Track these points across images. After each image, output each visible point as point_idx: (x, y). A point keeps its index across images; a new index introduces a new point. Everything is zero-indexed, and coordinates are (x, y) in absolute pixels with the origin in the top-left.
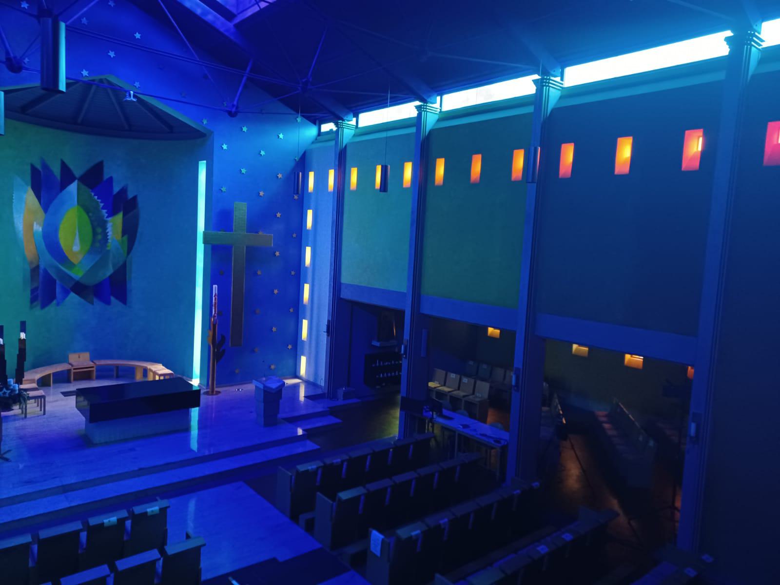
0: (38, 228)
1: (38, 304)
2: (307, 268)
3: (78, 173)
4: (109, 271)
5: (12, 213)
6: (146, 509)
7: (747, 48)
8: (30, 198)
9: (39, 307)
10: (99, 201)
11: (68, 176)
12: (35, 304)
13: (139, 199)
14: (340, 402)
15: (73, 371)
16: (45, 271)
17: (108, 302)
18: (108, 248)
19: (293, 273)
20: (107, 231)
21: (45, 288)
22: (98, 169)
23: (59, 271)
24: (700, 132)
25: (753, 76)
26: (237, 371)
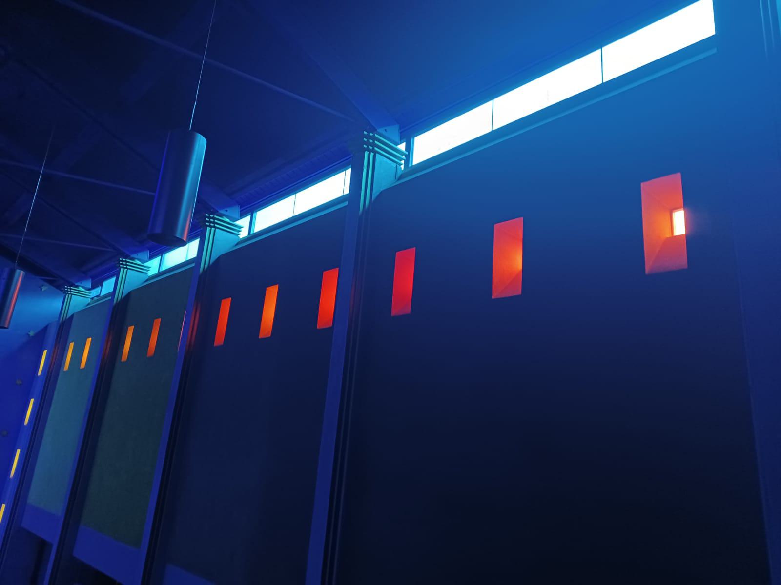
2: (10, 479)
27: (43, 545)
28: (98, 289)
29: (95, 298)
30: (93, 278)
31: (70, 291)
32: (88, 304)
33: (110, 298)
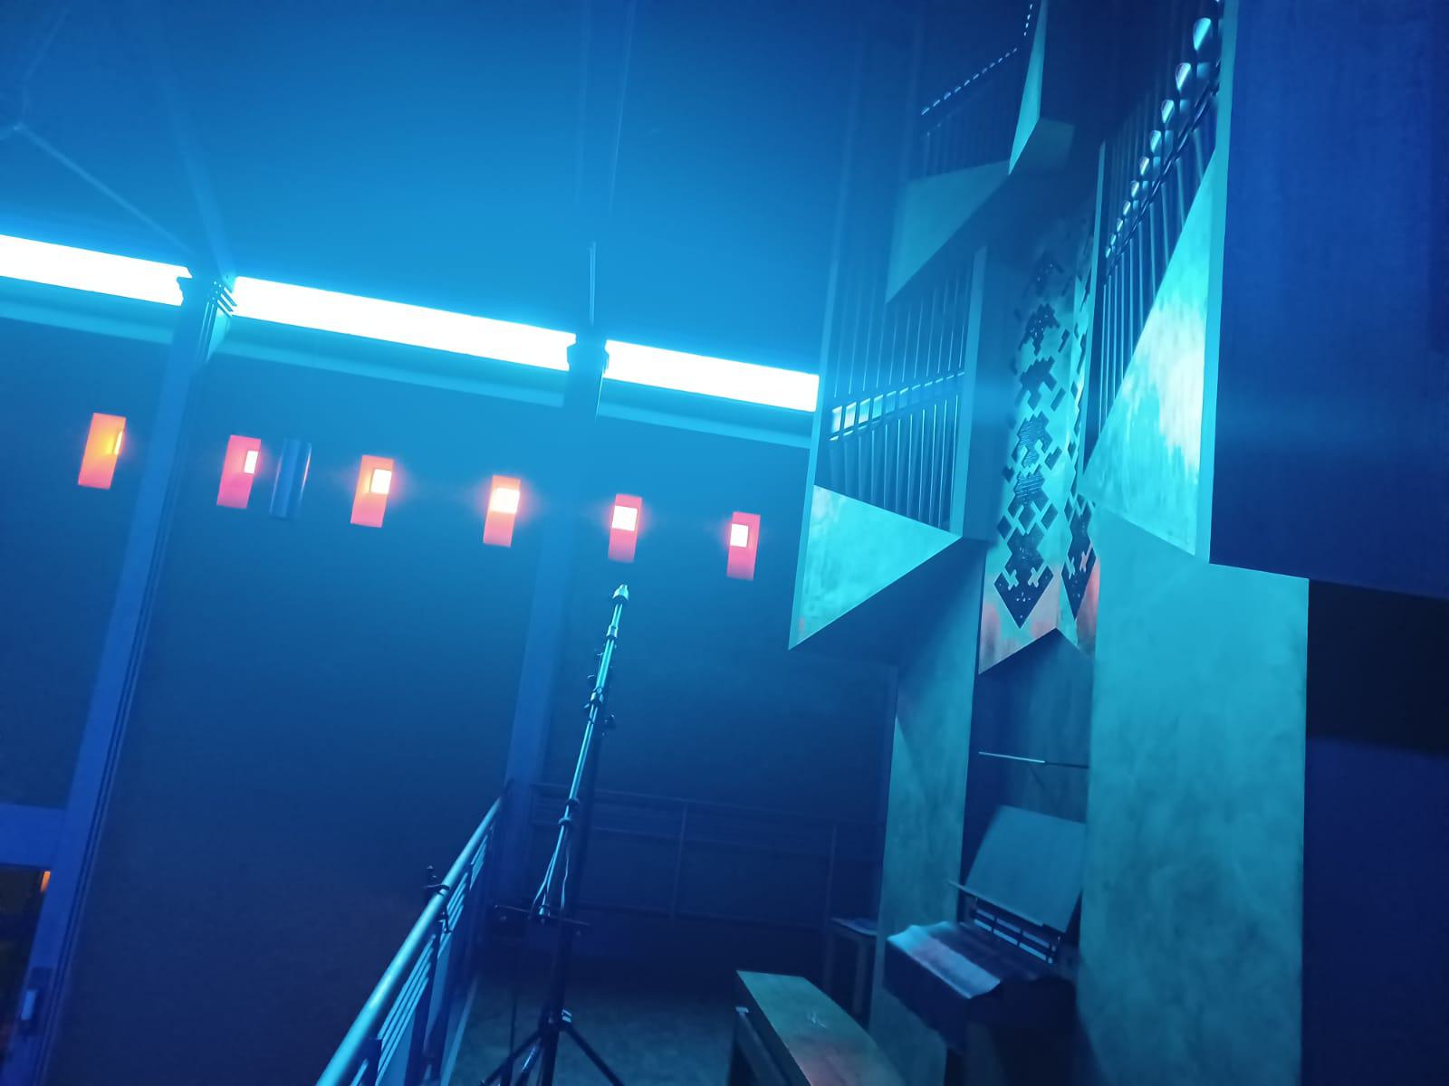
7: (210, 306)
24: (120, 423)
25: (215, 355)
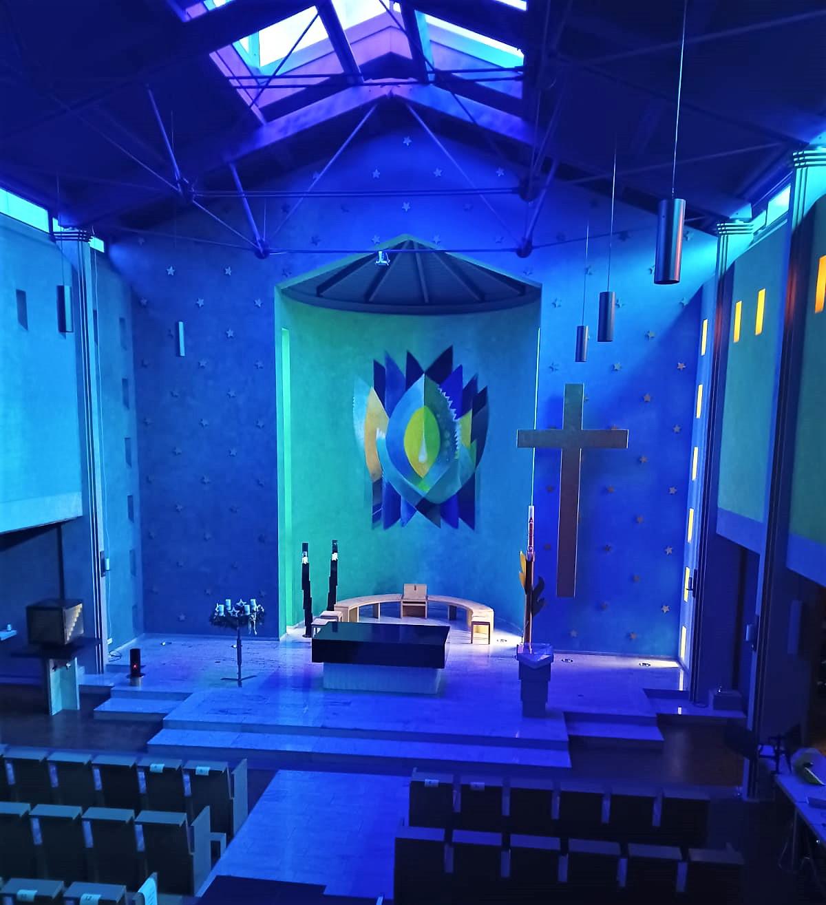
0: (381, 435)
1: (381, 523)
2: (693, 482)
3: (425, 364)
4: (457, 487)
5: (352, 419)
6: (196, 766)
8: (372, 400)
9: (382, 526)
10: (448, 397)
11: (414, 371)
12: (379, 522)
13: (489, 392)
14: (710, 711)
15: (402, 604)
16: (389, 486)
17: (455, 525)
18: (457, 457)
19: (672, 490)
20: (456, 436)
21: (388, 505)
22: (446, 358)
23: (404, 485)
26: (574, 634)
27: (746, 557)
28: (763, 215)
29: (760, 232)
30: (752, 201)
31: (803, 161)
32: (752, 243)
33: (786, 221)
